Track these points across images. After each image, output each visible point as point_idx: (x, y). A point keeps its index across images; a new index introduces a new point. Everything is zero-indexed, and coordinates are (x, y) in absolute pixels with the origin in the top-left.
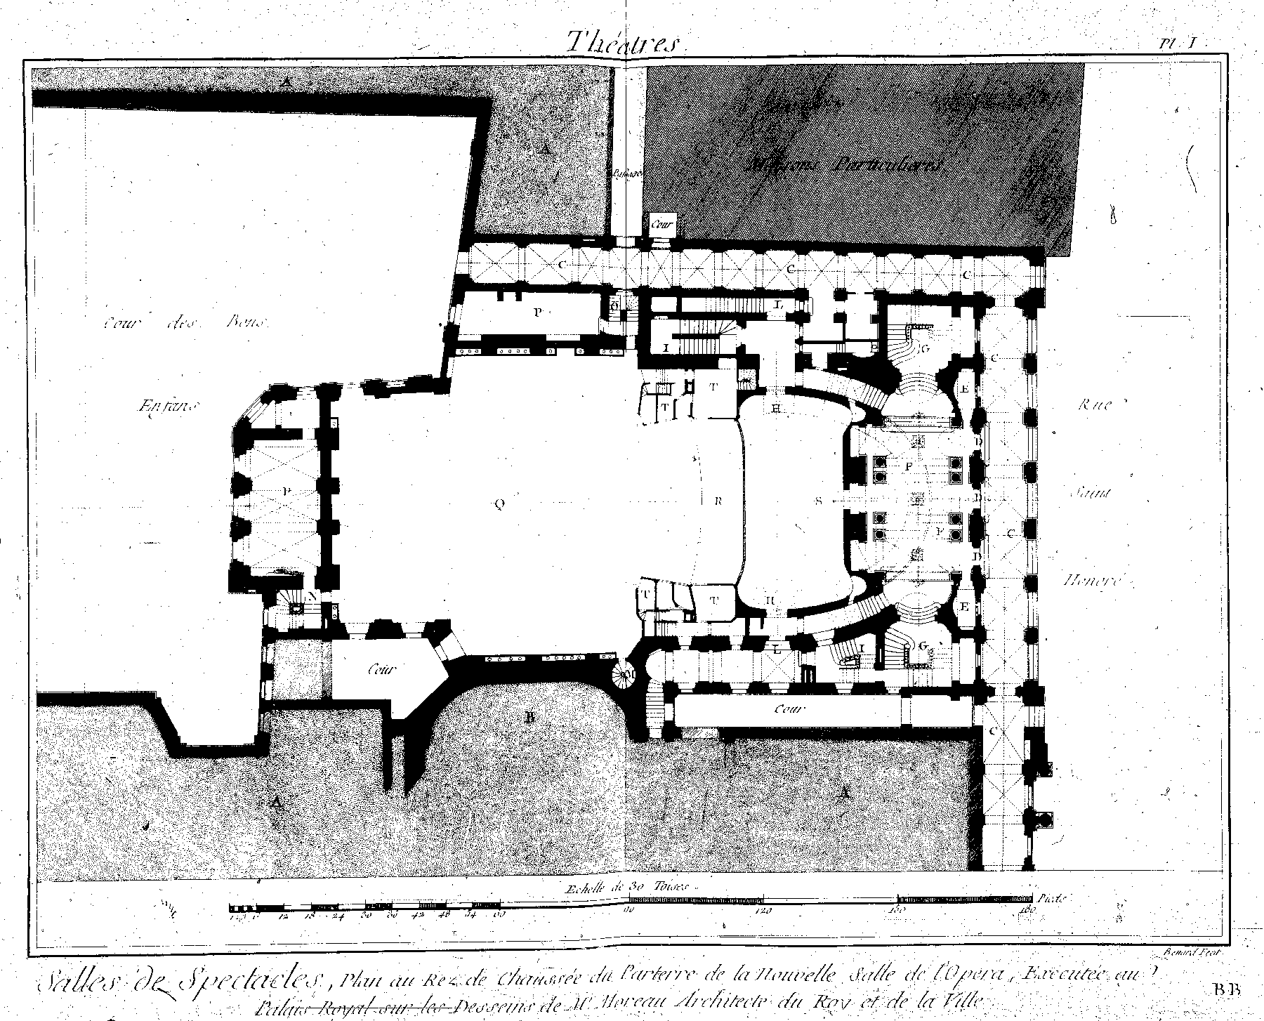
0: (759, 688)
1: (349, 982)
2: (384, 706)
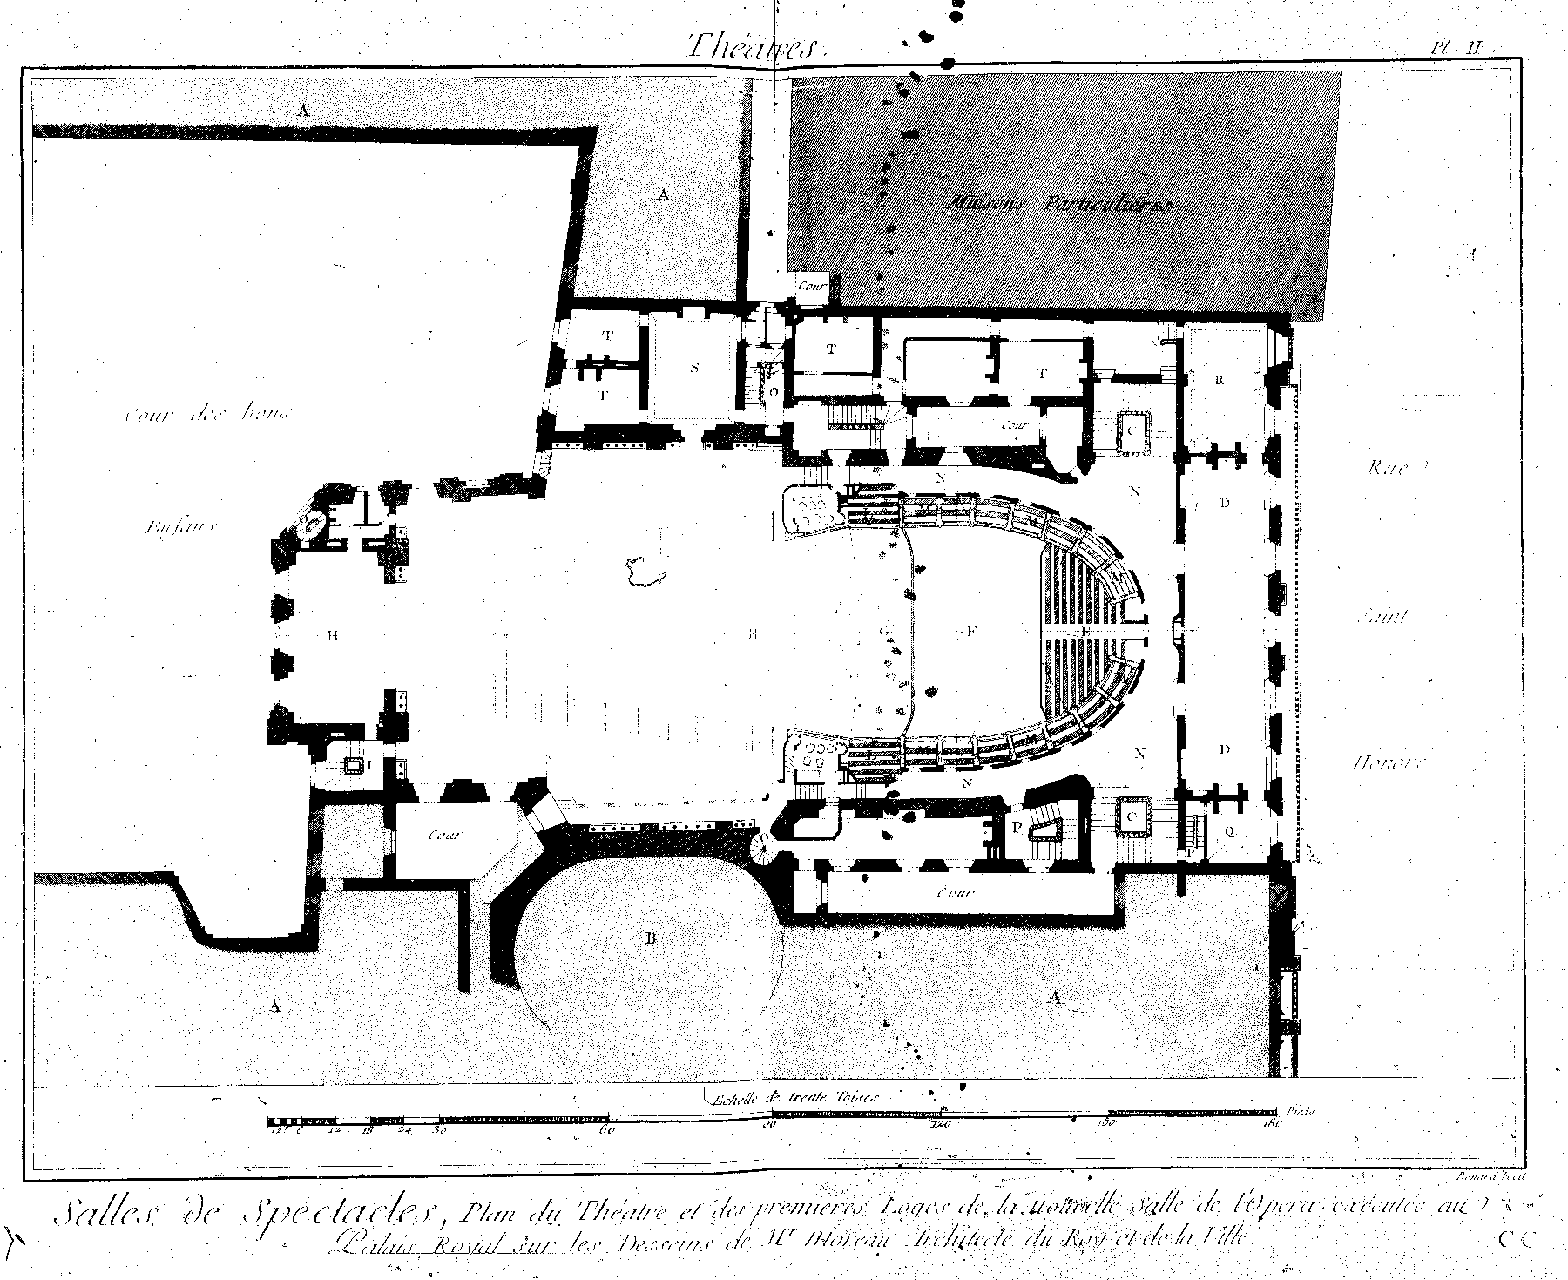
1: (476, 1214)
2: (461, 887)
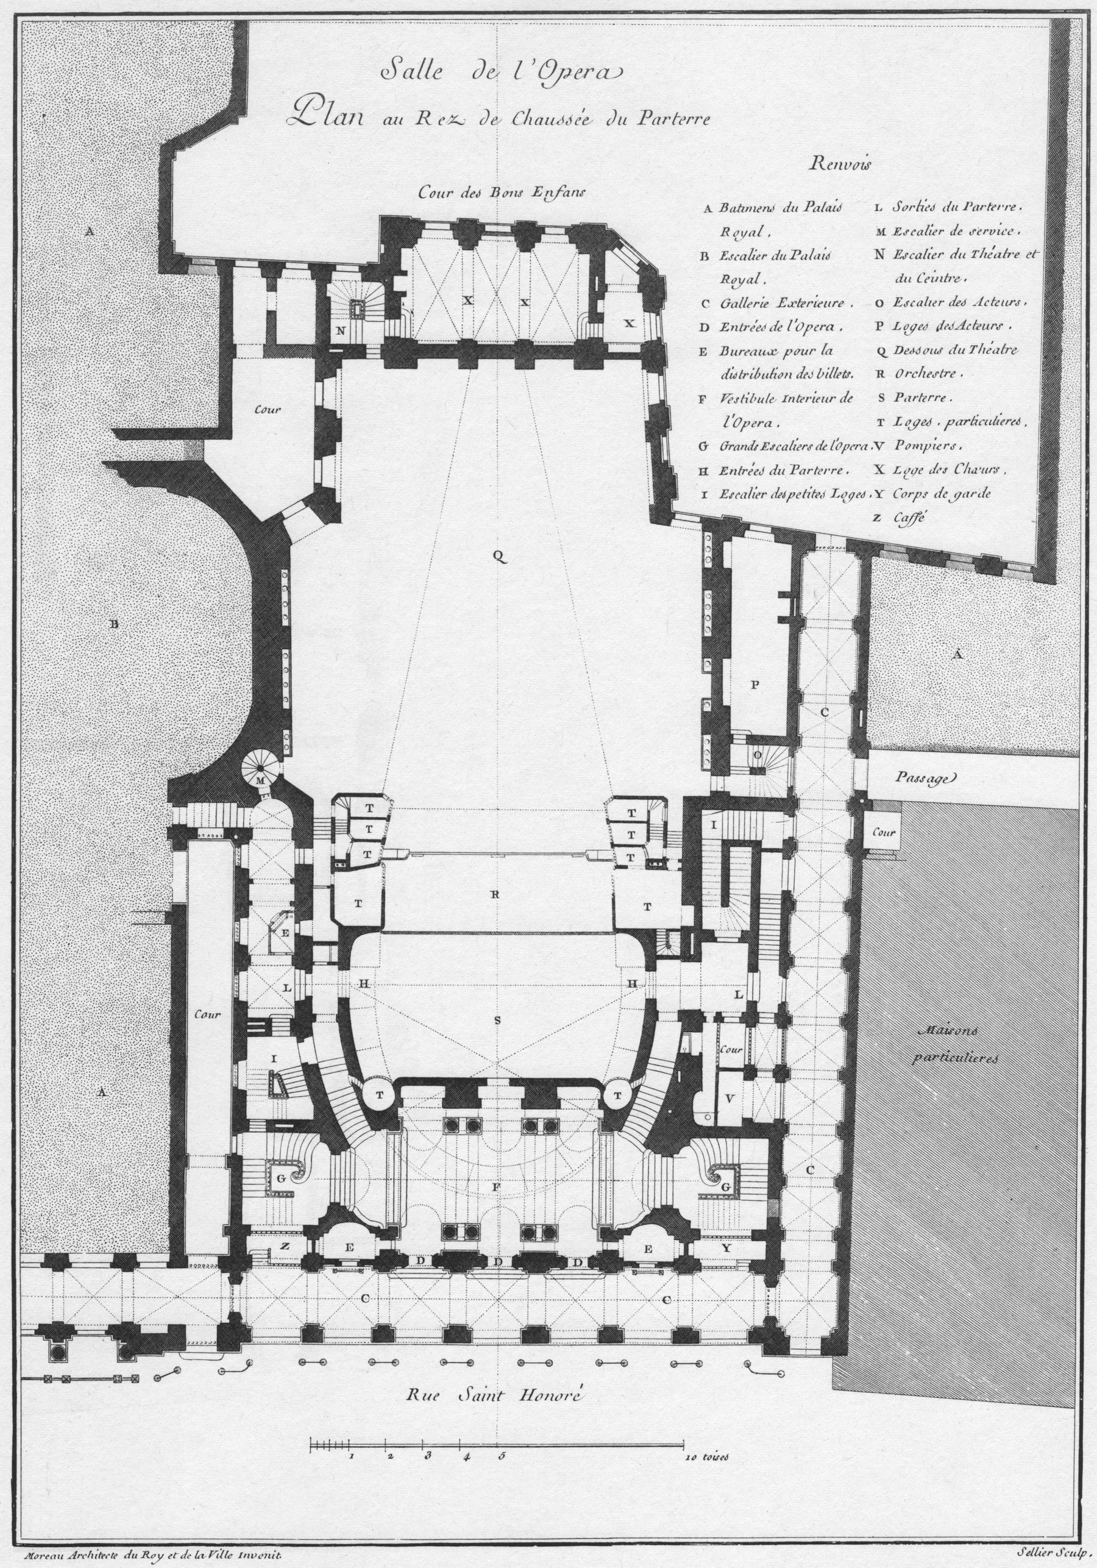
0: (242, 958)
2: (224, 431)
